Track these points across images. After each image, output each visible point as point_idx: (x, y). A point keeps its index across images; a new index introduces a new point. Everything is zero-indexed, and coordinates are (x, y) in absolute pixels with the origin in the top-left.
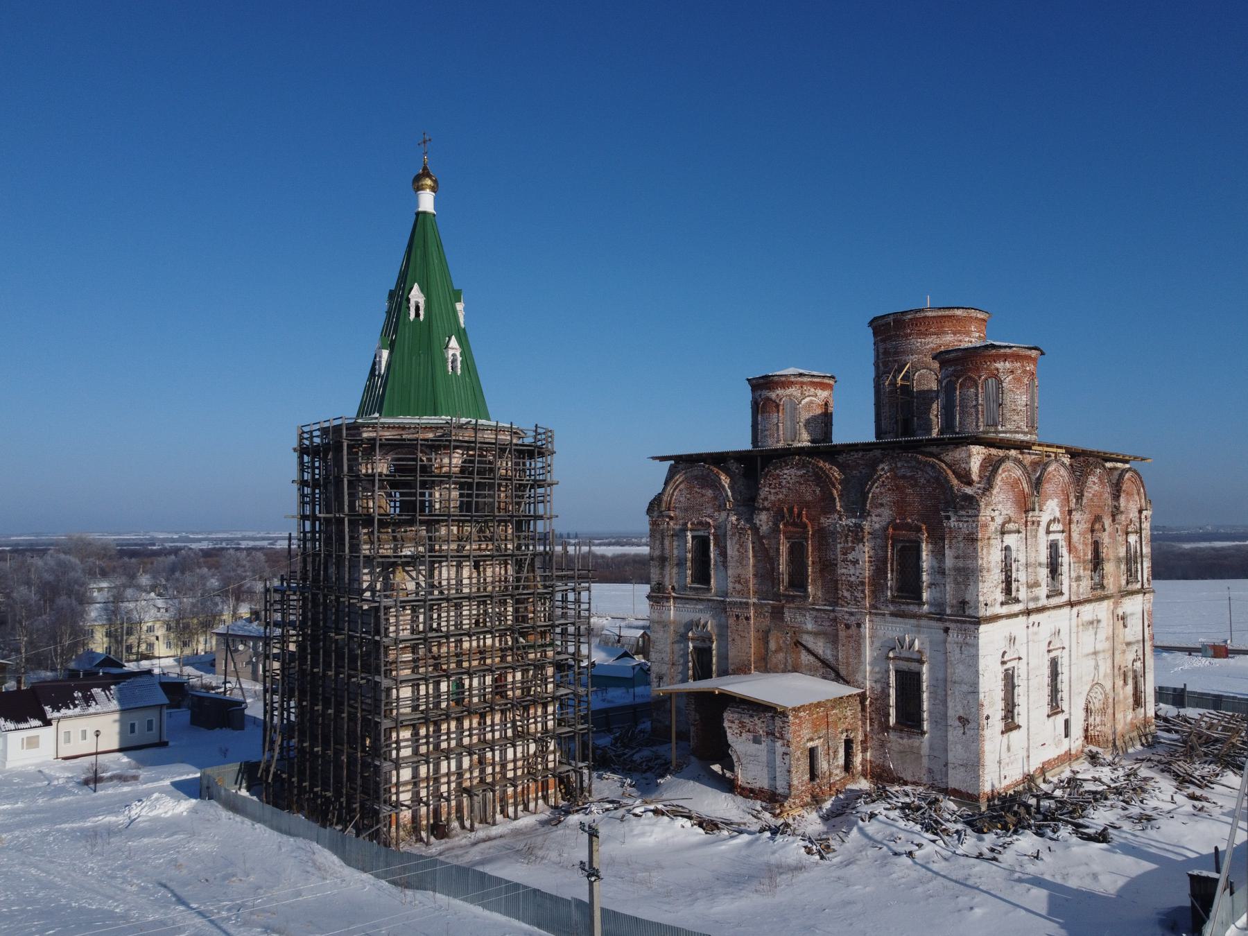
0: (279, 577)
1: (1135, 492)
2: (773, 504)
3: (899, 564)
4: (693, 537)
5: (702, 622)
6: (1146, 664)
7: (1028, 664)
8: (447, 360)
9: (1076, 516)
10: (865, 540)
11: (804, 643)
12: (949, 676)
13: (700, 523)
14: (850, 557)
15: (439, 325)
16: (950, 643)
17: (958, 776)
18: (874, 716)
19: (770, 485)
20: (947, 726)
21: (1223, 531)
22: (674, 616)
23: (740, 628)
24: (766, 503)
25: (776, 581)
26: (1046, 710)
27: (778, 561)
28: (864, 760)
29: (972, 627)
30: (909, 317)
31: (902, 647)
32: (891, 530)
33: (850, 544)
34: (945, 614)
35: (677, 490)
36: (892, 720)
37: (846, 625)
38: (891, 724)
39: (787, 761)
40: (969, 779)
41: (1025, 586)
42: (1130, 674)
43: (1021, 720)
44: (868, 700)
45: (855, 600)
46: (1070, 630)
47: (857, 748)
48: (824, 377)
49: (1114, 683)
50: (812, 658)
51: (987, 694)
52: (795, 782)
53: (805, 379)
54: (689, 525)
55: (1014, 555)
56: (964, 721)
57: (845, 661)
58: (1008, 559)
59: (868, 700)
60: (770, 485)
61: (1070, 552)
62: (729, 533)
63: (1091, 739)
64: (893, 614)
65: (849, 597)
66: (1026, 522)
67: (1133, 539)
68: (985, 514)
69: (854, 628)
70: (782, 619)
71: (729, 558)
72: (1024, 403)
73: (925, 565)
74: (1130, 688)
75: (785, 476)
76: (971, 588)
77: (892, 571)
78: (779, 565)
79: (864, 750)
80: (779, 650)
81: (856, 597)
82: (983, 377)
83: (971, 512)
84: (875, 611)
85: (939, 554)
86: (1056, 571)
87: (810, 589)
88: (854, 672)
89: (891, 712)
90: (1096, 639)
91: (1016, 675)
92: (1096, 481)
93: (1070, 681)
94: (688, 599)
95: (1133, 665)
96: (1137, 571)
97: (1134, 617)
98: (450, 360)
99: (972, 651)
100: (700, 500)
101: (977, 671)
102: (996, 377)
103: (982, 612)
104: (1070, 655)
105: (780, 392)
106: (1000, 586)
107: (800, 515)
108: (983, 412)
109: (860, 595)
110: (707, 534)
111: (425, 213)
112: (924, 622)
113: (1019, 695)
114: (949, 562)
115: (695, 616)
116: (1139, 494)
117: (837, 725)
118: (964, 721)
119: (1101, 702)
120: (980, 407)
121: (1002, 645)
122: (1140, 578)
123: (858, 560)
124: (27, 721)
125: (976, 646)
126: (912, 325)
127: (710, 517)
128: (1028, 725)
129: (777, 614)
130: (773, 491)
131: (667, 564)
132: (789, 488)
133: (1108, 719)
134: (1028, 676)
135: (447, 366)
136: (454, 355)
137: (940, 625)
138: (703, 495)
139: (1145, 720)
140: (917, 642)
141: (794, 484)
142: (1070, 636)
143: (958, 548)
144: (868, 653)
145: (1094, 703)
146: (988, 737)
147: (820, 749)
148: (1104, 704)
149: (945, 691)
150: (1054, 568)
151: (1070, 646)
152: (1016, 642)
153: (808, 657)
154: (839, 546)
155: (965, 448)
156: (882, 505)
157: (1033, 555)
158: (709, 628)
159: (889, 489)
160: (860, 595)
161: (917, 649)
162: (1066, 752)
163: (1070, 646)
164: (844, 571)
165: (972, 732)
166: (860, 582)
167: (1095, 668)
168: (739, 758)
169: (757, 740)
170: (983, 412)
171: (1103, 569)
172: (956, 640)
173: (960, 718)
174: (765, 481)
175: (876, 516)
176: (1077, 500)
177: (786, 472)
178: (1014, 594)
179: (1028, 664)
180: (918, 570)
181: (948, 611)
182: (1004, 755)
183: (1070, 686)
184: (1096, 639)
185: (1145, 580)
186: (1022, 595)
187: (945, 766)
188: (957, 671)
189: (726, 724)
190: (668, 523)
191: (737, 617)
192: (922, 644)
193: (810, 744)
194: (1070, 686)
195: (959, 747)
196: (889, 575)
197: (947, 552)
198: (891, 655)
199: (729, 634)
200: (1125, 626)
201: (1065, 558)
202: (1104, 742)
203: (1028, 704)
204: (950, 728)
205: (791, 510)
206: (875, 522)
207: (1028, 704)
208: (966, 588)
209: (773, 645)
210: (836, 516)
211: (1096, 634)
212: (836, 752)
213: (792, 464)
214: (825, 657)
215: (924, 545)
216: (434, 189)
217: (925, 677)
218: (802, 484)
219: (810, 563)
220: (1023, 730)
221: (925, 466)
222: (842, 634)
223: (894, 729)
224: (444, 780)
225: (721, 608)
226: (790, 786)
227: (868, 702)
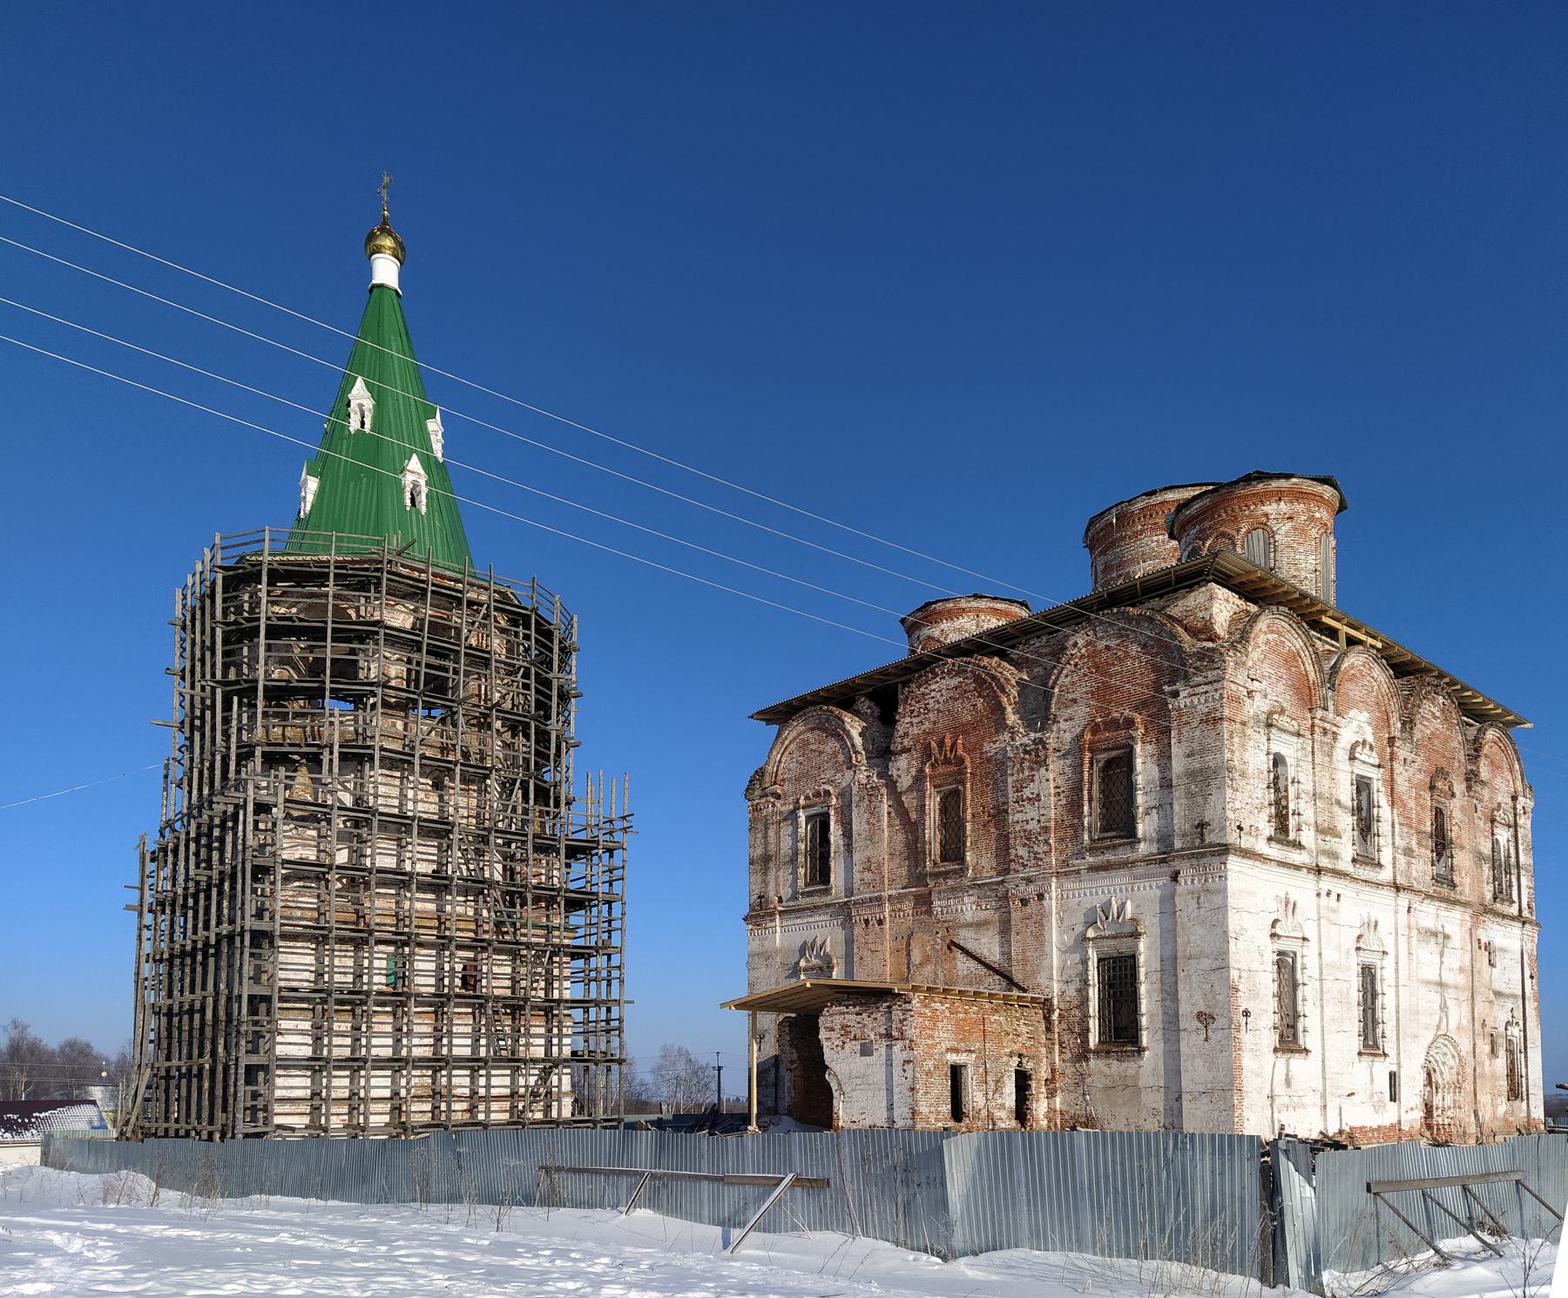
1: (1506, 766)
2: (916, 740)
3: (1102, 792)
4: (809, 819)
5: (819, 943)
6: (1528, 1034)
7: (1320, 954)
8: (401, 490)
9: (1403, 752)
10: (1049, 761)
11: (962, 943)
12: (1180, 948)
13: (817, 794)
14: (1027, 793)
16: (1180, 895)
17: (1199, 1112)
19: (912, 712)
20: (1178, 1030)
22: (782, 941)
23: (870, 938)
24: (906, 742)
25: (921, 856)
26: (1356, 1043)
27: (924, 824)
28: (1051, 1110)
29: (1216, 860)
30: (1140, 505)
31: (1107, 918)
32: (1088, 736)
33: (1026, 773)
34: (1173, 850)
35: (786, 753)
36: (1093, 1039)
37: (1022, 901)
38: (1092, 1046)
39: (909, 1074)
40: (1216, 1114)
41: (1312, 829)
42: (1501, 1041)
43: (1309, 1040)
44: (1057, 1013)
45: (1035, 858)
46: (1396, 929)
47: (1038, 1088)
49: (1475, 1044)
50: (973, 964)
51: (1244, 974)
52: (923, 1109)
53: (983, 604)
54: (802, 802)
55: (1291, 773)
56: (1205, 1018)
57: (1020, 957)
58: (1282, 779)
59: (1057, 1013)
60: (912, 712)
61: (1393, 804)
62: (855, 799)
63: (1438, 1129)
64: (1093, 869)
65: (1026, 855)
66: (1313, 726)
67: (1503, 835)
68: (1236, 677)
69: (1033, 904)
70: (929, 912)
71: (855, 836)
72: (1312, 568)
73: (1140, 780)
74: (1501, 1063)
75: (933, 694)
77: (1090, 800)
78: (924, 829)
79: (1051, 1094)
80: (926, 960)
81: (1036, 853)
82: (1244, 530)
83: (1211, 675)
84: (1066, 872)
85: (1164, 758)
86: (1369, 828)
87: (969, 856)
89: (1091, 1025)
90: (1442, 963)
91: (1299, 966)
92: (1438, 714)
93: (1398, 1012)
94: (798, 910)
95: (1506, 1029)
96: (1511, 886)
97: (1508, 956)
98: (408, 489)
99: (1217, 900)
100: (816, 761)
101: (1226, 933)
103: (1232, 838)
104: (1397, 970)
105: (945, 625)
106: (1267, 811)
107: (954, 745)
109: (1042, 848)
110: (826, 809)
111: (381, 286)
112: (1140, 870)
113: (1304, 1000)
114: (1178, 765)
115: (808, 935)
116: (1511, 770)
117: (1000, 1042)
118: (1205, 1018)
119: (1454, 1071)
121: (1274, 909)
122: (1515, 897)
123: (1038, 795)
125: (1223, 891)
126: (1145, 517)
127: (830, 782)
128: (1323, 1054)
129: (924, 902)
130: (915, 720)
131: (771, 865)
132: (938, 711)
133: (1465, 1099)
134: (1321, 973)
135: (402, 498)
136: (415, 485)
137: (1165, 868)
138: (820, 753)
139: (1528, 1122)
140: (1129, 904)
141: (946, 702)
142: (1396, 940)
143: (1192, 740)
144: (1056, 937)
145: (1442, 1073)
146: (1248, 1046)
147: (970, 1070)
148: (1458, 1074)
149: (1176, 975)
150: (1366, 827)
151: (1397, 951)
152: (1297, 911)
154: (1010, 780)
155: (1203, 589)
156: (1075, 701)
157: (1326, 782)
158: (828, 950)
160: (1042, 848)
161: (1129, 916)
162: (1392, 1125)
163: (1397, 951)
164: (1018, 817)
165: (1220, 1034)
166: (1041, 828)
167: (1441, 1009)
168: (839, 1084)
169: (866, 1051)
171: (1452, 857)
172: (1190, 887)
173: (1200, 1015)
174: (905, 709)
175: (1066, 720)
176: (1404, 724)
177: (933, 687)
178: (1292, 836)
179: (1320, 954)
180: (1131, 788)
181: (1178, 844)
182: (1280, 1089)
183: (1398, 1020)
184: (1442, 963)
185: (1524, 905)
186: (1308, 837)
187: (1177, 1100)
189: (823, 1035)
190: (774, 805)
191: (867, 922)
192: (1138, 906)
193: (952, 1058)
194: (1398, 1020)
195: (1199, 1062)
196: (1086, 808)
197: (1174, 750)
198: (1091, 933)
199: (856, 950)
200: (1491, 964)
201: (1384, 812)
202: (1459, 1136)
203: (1322, 1019)
204: (1183, 1034)
205: (941, 744)
206: (1063, 733)
207: (1322, 1019)
208: (1205, 799)
209: (916, 956)
210: (1007, 736)
211: (1442, 955)
212: (999, 1082)
213: (943, 672)
215: (1138, 748)
217: (1142, 959)
218: (956, 700)
219: (969, 817)
220: (1314, 1058)
221: (1138, 623)
222: (1016, 916)
223: (1096, 1052)
224: (293, 1085)
225: (844, 911)
226: (914, 1113)
227: (1055, 1017)
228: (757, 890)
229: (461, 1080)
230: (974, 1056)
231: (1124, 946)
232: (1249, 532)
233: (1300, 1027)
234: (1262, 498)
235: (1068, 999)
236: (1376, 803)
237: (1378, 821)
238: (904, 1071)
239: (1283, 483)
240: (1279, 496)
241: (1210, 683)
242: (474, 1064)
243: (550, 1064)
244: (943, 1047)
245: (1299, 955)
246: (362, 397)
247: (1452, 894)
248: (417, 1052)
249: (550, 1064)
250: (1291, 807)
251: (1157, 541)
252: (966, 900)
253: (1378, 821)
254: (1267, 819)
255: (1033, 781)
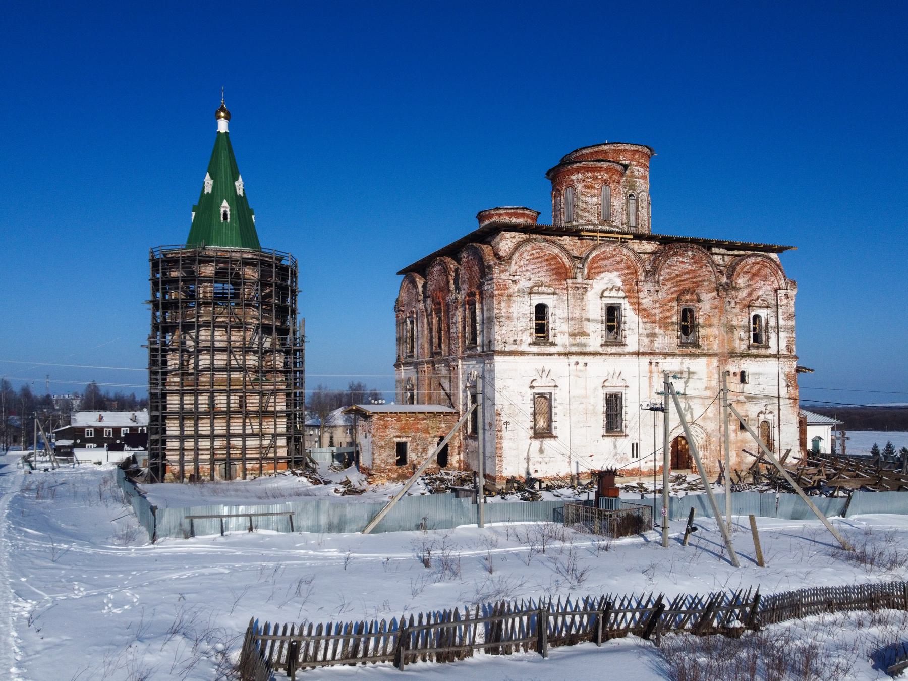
15: (219, 194)
30: (573, 156)
48: (517, 209)
53: (502, 212)
76: (492, 330)
102: (572, 186)
108: (564, 213)
120: (562, 210)
124: (137, 447)
147: (408, 445)
170: (564, 213)
171: (698, 332)
178: (551, 340)
193: (398, 440)
216: (226, 118)
224: (173, 444)
229: (237, 442)
230: (410, 439)
232: (566, 189)
233: (553, 426)
234: (571, 172)
236: (623, 315)
237: (625, 323)
239: (579, 165)
240: (578, 171)
242: (244, 436)
243: (275, 436)
244: (392, 436)
245: (553, 394)
246: (208, 180)
247: (699, 351)
248: (236, 432)
249: (275, 436)
250: (551, 326)
253: (625, 323)
254: (529, 335)
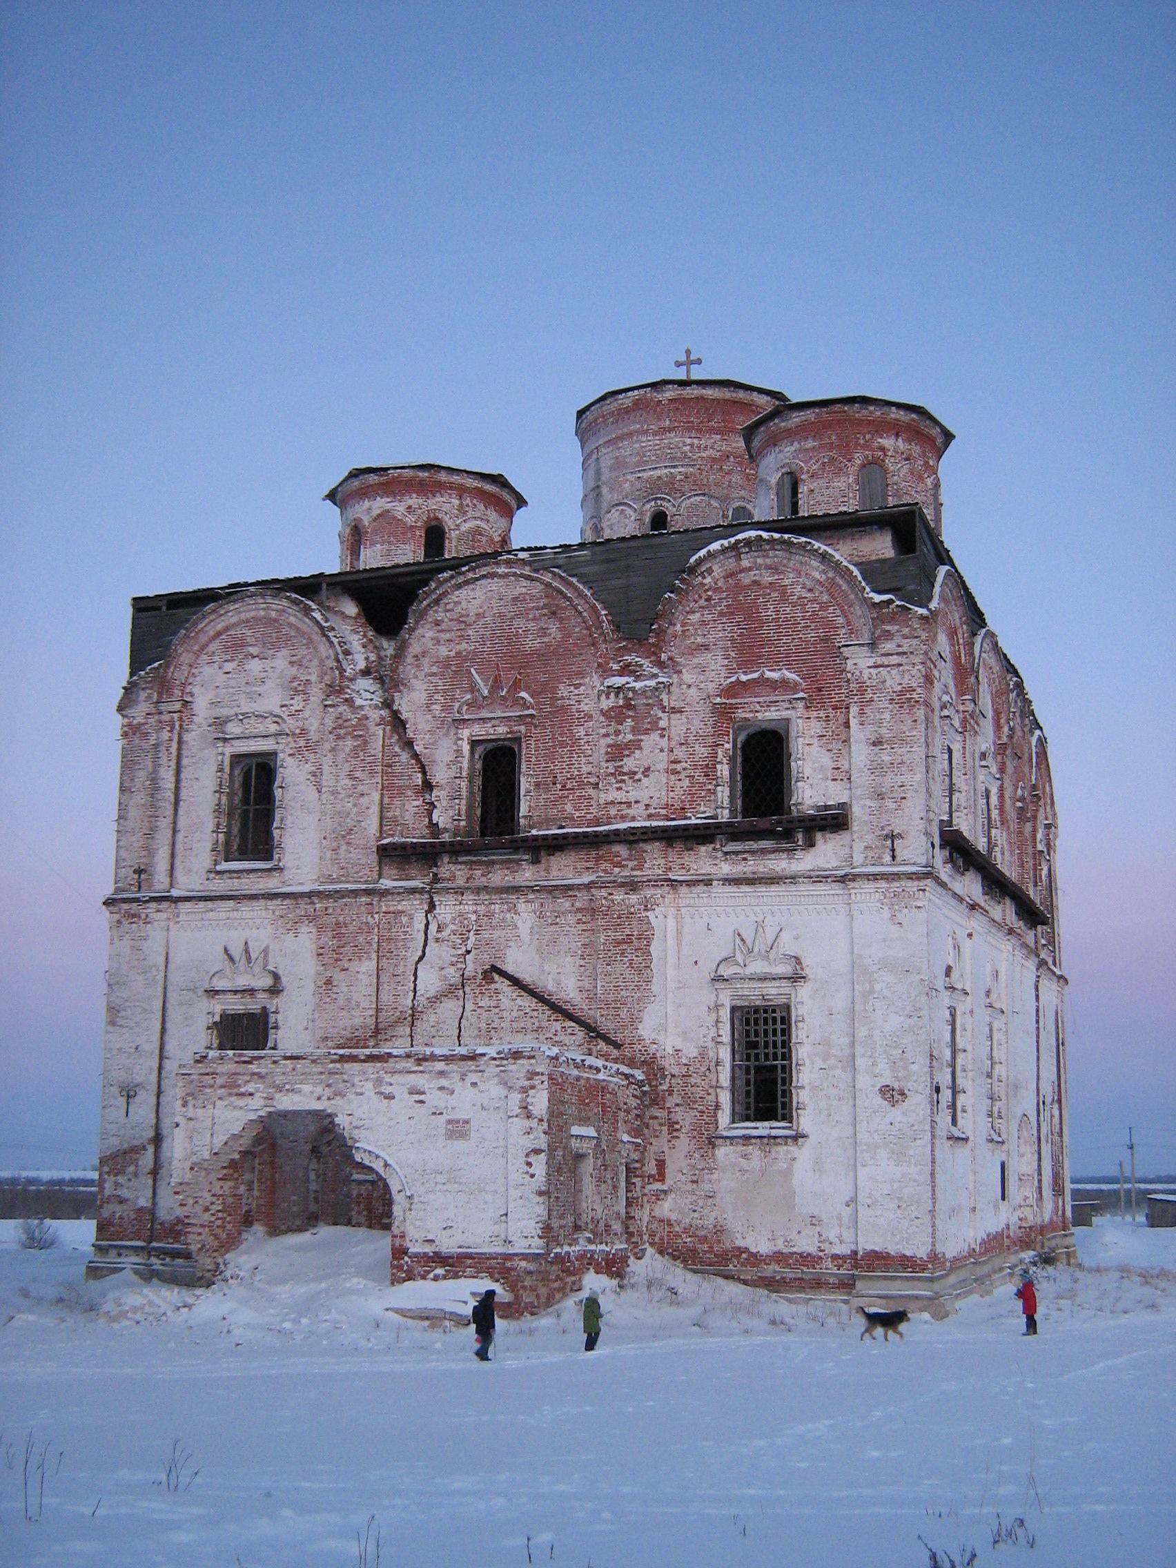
0: (95, 1285)
18: (582, 1082)
21: (902, 413)
50: (527, 1002)
88: (633, 1021)
153: (519, 1002)
159: (721, 614)
188: (877, 987)
214: (562, 995)
228: (132, 860)
231: (774, 992)
235: (684, 1061)
238: (529, 1164)
241: (905, 653)
251: (692, 445)
252: (521, 906)
255: (640, 748)
